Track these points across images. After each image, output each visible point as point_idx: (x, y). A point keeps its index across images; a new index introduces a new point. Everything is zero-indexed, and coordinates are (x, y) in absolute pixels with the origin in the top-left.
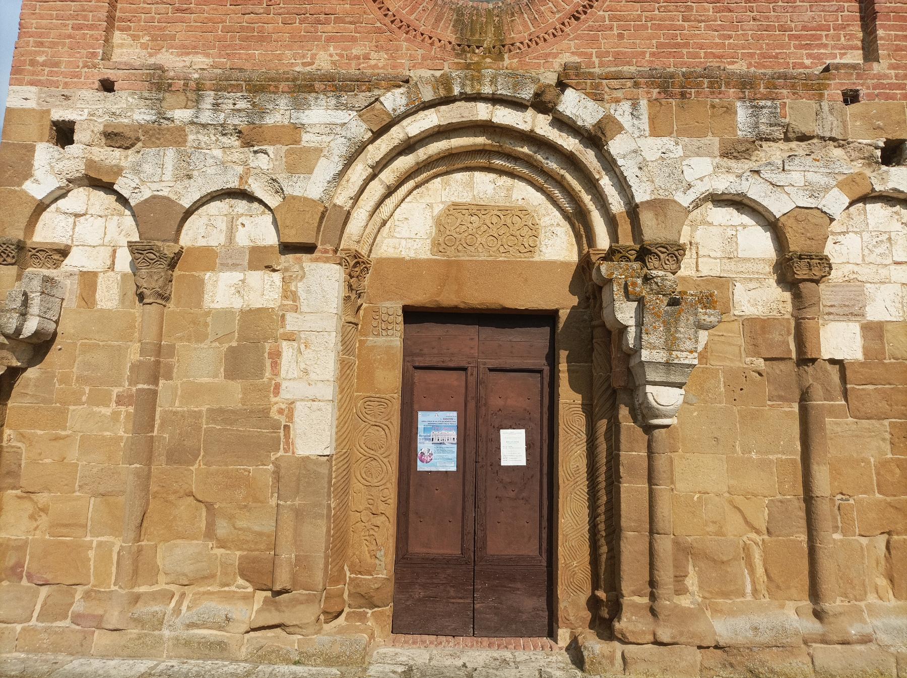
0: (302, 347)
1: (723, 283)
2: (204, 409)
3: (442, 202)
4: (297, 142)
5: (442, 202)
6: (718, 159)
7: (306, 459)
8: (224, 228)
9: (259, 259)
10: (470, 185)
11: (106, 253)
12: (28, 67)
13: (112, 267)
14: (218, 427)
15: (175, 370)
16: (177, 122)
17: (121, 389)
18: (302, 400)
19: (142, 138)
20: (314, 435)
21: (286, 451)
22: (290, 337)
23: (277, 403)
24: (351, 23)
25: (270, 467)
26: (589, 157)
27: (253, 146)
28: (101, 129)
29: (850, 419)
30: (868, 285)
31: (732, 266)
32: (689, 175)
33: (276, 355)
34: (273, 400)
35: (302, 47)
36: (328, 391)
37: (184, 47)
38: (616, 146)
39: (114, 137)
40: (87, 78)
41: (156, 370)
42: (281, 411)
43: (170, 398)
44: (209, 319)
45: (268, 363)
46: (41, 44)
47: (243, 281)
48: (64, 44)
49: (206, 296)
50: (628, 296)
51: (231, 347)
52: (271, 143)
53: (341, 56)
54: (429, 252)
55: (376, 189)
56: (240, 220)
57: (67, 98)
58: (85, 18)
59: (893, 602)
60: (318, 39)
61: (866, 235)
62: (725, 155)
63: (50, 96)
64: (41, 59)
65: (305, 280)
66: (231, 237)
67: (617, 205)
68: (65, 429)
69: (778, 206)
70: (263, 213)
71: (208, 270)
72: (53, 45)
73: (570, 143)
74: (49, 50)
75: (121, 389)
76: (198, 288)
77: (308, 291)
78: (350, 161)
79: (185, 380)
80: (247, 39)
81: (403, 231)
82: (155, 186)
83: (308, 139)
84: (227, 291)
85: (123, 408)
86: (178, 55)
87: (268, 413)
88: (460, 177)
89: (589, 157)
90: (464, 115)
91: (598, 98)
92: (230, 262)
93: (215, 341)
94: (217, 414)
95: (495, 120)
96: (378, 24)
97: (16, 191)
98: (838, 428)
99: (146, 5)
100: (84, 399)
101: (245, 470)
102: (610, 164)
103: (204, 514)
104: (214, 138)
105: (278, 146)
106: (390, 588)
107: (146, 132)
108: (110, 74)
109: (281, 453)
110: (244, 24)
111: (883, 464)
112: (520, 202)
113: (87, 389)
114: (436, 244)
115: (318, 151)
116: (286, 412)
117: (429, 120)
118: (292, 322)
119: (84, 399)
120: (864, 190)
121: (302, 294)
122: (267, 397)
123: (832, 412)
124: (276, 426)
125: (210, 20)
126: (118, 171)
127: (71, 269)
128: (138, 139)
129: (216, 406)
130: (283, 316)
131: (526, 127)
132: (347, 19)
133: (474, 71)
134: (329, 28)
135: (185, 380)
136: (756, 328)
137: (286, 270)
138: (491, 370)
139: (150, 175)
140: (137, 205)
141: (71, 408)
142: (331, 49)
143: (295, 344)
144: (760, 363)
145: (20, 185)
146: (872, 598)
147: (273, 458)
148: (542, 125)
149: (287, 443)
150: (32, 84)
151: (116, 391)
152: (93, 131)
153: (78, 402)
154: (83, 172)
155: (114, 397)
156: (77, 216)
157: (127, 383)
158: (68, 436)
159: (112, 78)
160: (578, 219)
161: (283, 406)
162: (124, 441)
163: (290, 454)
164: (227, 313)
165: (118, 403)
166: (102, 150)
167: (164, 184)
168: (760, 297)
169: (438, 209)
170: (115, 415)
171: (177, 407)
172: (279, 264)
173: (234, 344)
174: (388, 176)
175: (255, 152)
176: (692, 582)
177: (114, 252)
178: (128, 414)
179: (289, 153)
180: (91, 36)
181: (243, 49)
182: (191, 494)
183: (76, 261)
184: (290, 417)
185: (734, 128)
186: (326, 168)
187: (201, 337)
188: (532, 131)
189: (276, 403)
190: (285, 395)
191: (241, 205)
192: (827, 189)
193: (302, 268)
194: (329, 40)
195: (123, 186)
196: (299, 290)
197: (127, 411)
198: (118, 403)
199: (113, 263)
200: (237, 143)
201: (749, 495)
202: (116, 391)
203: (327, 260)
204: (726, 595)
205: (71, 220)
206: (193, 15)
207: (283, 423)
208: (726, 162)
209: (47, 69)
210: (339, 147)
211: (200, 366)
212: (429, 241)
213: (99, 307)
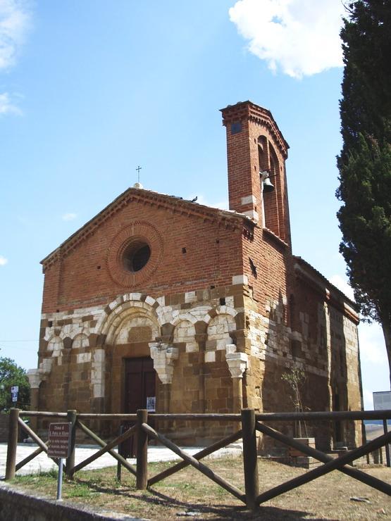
7: (96, 399)
9: (87, 350)
10: (136, 322)
22: (93, 369)
23: (91, 385)
31: (185, 339)
32: (174, 316)
33: (90, 373)
41: (68, 379)
43: (72, 387)
55: (112, 328)
76: (76, 358)
78: (104, 323)
81: (121, 337)
83: (95, 318)
84: (82, 358)
94: (81, 389)
98: (209, 380)
100: (15, 399)
114: (129, 340)
115: (96, 321)
118: (93, 365)
121: (140, 204)
124: (90, 391)
136: (191, 355)
139: (66, 331)
151: (62, 385)
164: (81, 364)
168: (191, 348)
171: (73, 387)
176: (174, 424)
183: (55, 354)
192: (205, 315)
211: (76, 377)
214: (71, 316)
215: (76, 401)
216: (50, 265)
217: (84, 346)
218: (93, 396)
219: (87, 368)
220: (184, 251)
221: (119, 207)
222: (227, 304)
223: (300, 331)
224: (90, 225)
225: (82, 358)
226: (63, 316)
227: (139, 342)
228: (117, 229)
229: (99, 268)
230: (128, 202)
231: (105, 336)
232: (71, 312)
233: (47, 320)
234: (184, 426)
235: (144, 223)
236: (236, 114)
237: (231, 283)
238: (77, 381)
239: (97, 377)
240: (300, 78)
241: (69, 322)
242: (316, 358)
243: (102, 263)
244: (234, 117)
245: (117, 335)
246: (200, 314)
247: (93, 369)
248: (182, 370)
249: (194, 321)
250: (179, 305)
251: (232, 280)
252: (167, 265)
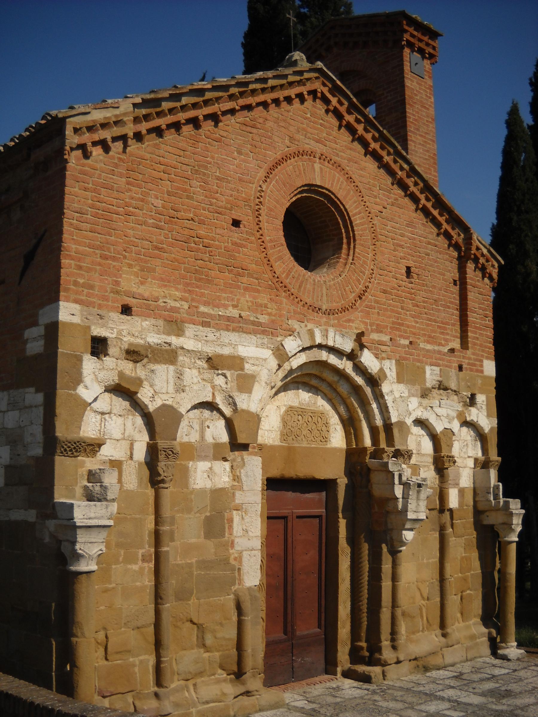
0: (244, 514)
2: (194, 560)
3: (285, 405)
4: (242, 369)
5: (285, 405)
6: (420, 399)
7: (249, 589)
8: (198, 429)
11: (125, 445)
12: (72, 287)
13: (131, 458)
14: (203, 573)
15: (176, 535)
16: (173, 347)
17: (144, 551)
18: (246, 550)
19: (150, 356)
20: (252, 575)
21: (239, 584)
24: (257, 279)
25: (232, 596)
26: (368, 391)
27: (218, 370)
28: (126, 347)
29: (454, 538)
30: (461, 469)
33: (231, 521)
34: (231, 551)
35: (231, 293)
36: (257, 543)
37: (162, 280)
38: (385, 388)
39: (133, 354)
40: (113, 302)
42: (235, 559)
44: (193, 496)
45: (227, 526)
46: (80, 268)
47: (211, 468)
48: (96, 271)
49: (190, 479)
50: (400, 483)
51: (206, 516)
52: (229, 369)
53: (252, 302)
54: (279, 441)
56: (207, 423)
57: (101, 317)
58: (109, 250)
60: (239, 287)
61: (460, 442)
63: (90, 314)
64: (81, 281)
65: (245, 468)
66: (202, 437)
67: (379, 422)
68: (110, 583)
69: (439, 428)
70: (219, 418)
71: (191, 460)
72: (89, 270)
73: (360, 380)
74: (86, 274)
75: (144, 551)
76: (185, 472)
77: (247, 476)
79: (182, 541)
80: (200, 280)
82: (164, 397)
85: (146, 565)
86: (160, 286)
87: (229, 560)
89: (368, 391)
90: (317, 356)
92: (203, 454)
93: (197, 512)
94: (204, 564)
95: (329, 361)
96: (270, 283)
97: (72, 394)
99: (135, 240)
100: (121, 559)
101: (219, 600)
102: (379, 397)
103: (196, 632)
104: (193, 361)
105: (233, 371)
107: (152, 352)
109: (237, 586)
110: (197, 268)
112: (321, 408)
113: (122, 552)
114: (284, 436)
116: (238, 559)
119: (121, 559)
121: (244, 478)
122: (228, 550)
124: (233, 569)
125: (177, 260)
126: (139, 382)
127: (104, 458)
128: (147, 357)
129: (201, 558)
130: (234, 494)
131: (341, 367)
132: (255, 276)
134: (245, 279)
135: (182, 541)
137: (234, 460)
138: (298, 517)
140: (155, 410)
141: (114, 567)
142: (247, 296)
143: (239, 512)
145: (75, 389)
147: (233, 590)
148: (347, 366)
149: (240, 580)
150: (76, 301)
151: (141, 552)
152: (120, 348)
153: (117, 562)
154: (117, 382)
155: (140, 557)
156: (103, 414)
157: (147, 546)
158: (113, 588)
159: (130, 304)
160: (350, 424)
161: (236, 555)
162: (149, 588)
163: (241, 587)
164: (203, 491)
165: (143, 560)
166: (122, 362)
167: (169, 395)
170: (142, 569)
172: (230, 457)
173: (208, 514)
175: (218, 375)
177: (132, 445)
178: (150, 568)
179: (238, 376)
180: (114, 266)
181: (197, 287)
182: (191, 621)
183: (107, 451)
184: (240, 562)
187: (189, 510)
188: (344, 369)
189: (233, 554)
190: (237, 548)
191: (207, 413)
193: (243, 459)
194: (246, 289)
195: (145, 395)
196: (242, 475)
197: (148, 566)
198: (143, 560)
199: (132, 454)
200: (206, 366)
202: (141, 552)
203: (255, 454)
205: (99, 417)
206: (166, 254)
207: (237, 567)
209: (86, 291)
212: (279, 433)
213: (125, 489)
215: (193, 601)
217: (209, 438)
218: (240, 580)
222: (478, 406)
224: (405, 166)
225: (206, 475)
227: (305, 444)
229: (236, 223)
232: (175, 326)
233: (89, 328)
237: (482, 372)
238: (193, 540)
239: (248, 533)
240: (470, 429)
241: (169, 355)
243: (247, 219)
250: (417, 387)
251: (482, 366)
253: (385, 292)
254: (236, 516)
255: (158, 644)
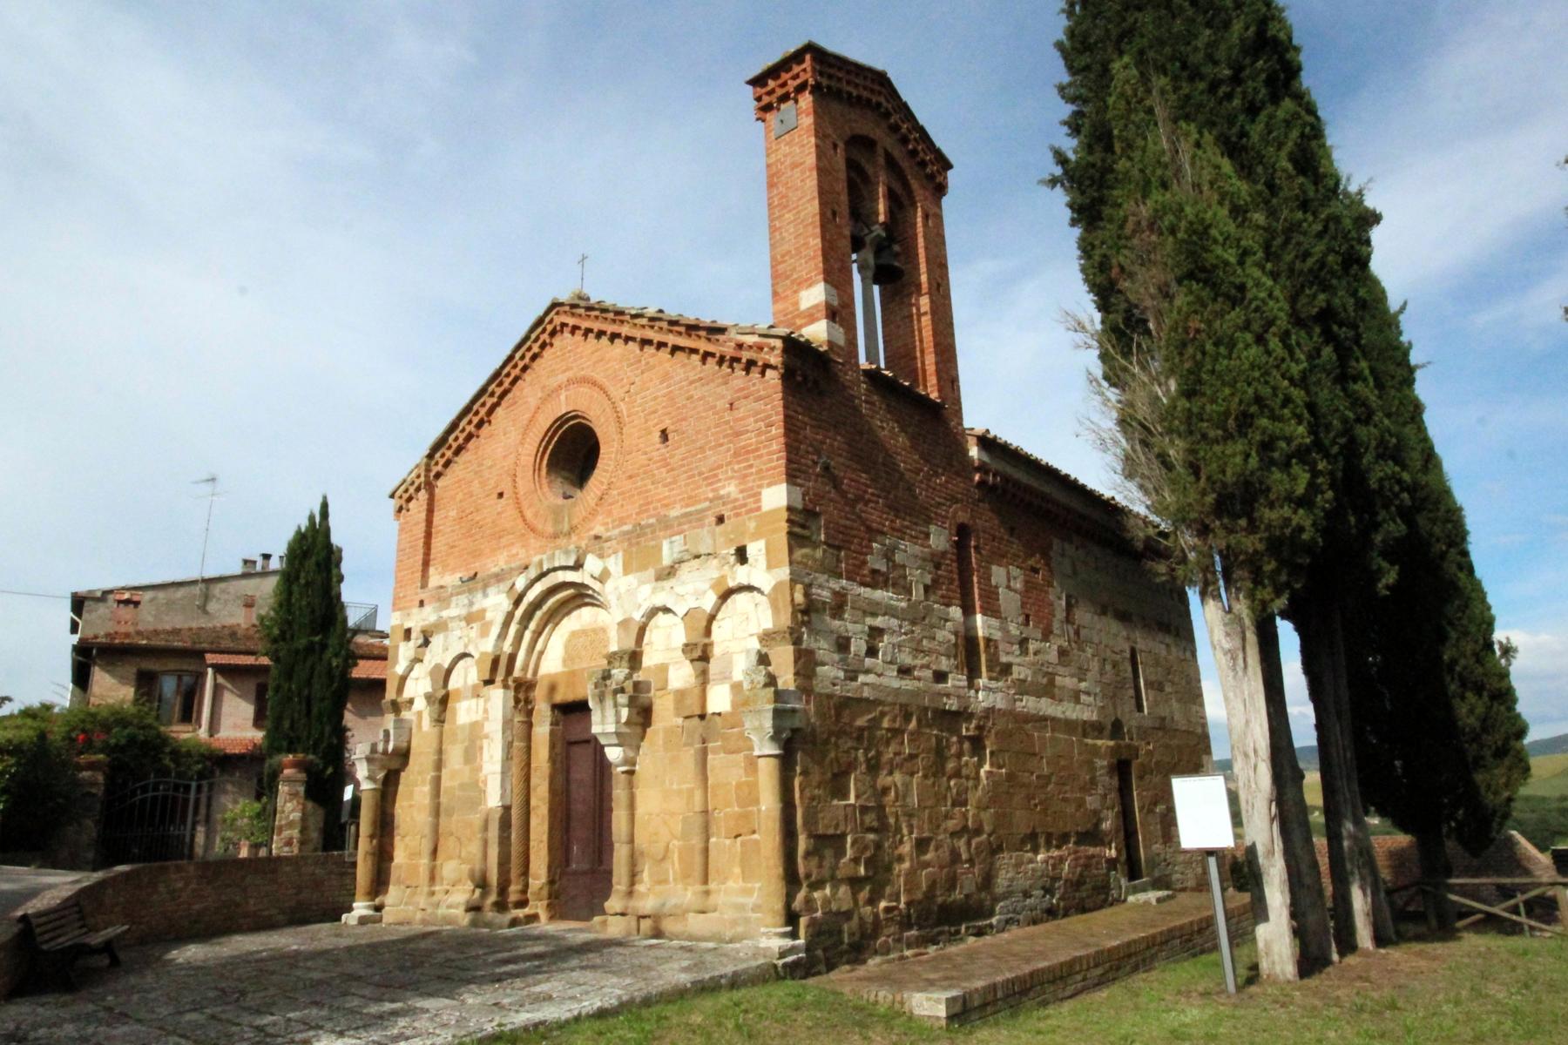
1: (663, 669)
22: (487, 737)
33: (481, 748)
59: (741, 883)
62: (659, 578)
83: (489, 616)
88: (575, 614)
91: (601, 556)
94: (462, 786)
106: (545, 892)
108: (423, 596)
111: (739, 786)
117: (539, 588)
120: (722, 589)
123: (715, 752)
133: (552, 557)
136: (681, 695)
144: (680, 721)
146: (731, 884)
164: (463, 727)
169: (566, 636)
174: (533, 625)
176: (646, 875)
185: (660, 559)
186: (495, 630)
201: (672, 814)
204: (659, 882)
208: (660, 584)
210: (499, 619)
214: (445, 614)
215: (455, 818)
216: (410, 499)
219: (475, 732)
220: (664, 435)
221: (536, 349)
223: (991, 610)
225: (465, 712)
226: (428, 615)
228: (533, 402)
229: (501, 495)
230: (553, 334)
231: (512, 658)
234: (666, 881)
235: (584, 380)
236: (784, 85)
237: (759, 509)
238: (457, 767)
242: (1051, 677)
243: (506, 486)
244: (780, 92)
245: (541, 653)
246: (693, 589)
247: (487, 737)
248: (661, 735)
249: (681, 610)
251: (759, 501)
252: (630, 477)
253: (630, 477)
254: (485, 742)
255: (434, 852)
